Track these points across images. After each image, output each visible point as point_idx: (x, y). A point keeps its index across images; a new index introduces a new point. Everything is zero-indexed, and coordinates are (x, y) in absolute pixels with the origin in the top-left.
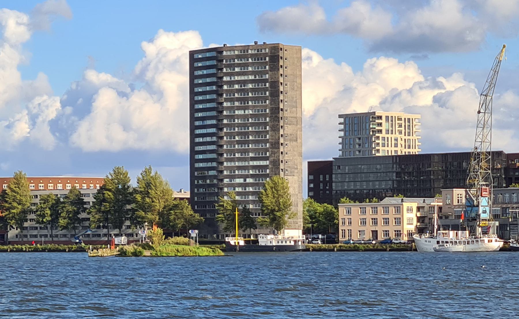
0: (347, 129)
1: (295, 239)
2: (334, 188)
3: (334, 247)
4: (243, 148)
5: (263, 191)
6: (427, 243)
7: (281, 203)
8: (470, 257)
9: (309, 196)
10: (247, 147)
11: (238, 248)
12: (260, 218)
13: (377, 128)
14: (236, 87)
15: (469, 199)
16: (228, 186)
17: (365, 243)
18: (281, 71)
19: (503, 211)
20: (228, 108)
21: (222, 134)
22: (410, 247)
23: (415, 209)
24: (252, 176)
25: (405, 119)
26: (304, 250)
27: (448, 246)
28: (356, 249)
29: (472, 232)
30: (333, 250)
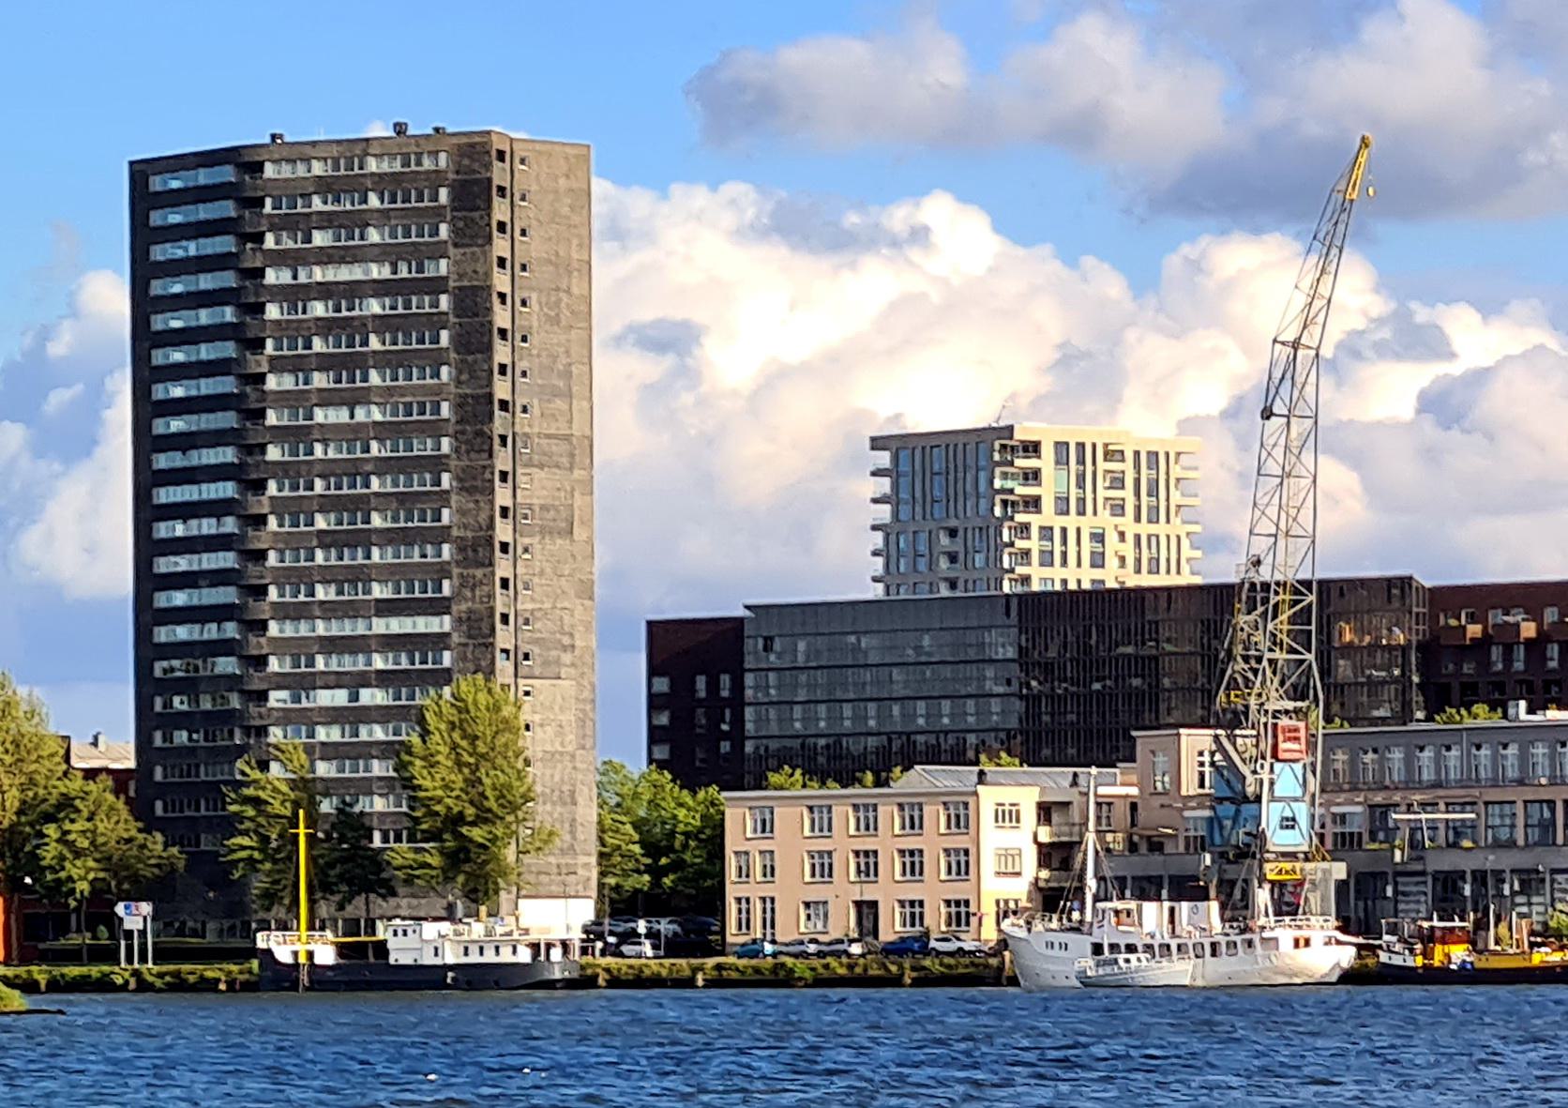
0: (904, 495)
1: (533, 937)
2: (749, 726)
3: (695, 970)
4: (346, 562)
5: (416, 740)
6: (1056, 952)
7: (489, 793)
8: (1209, 1011)
9: (651, 761)
10: (360, 561)
11: (304, 978)
12: (401, 852)
13: (1021, 490)
14: (318, 309)
15: (1227, 774)
16: (286, 718)
17: (820, 955)
18: (500, 246)
19: (1372, 820)
20: (284, 398)
21: (260, 505)
22: (988, 972)
23: (1029, 815)
24: (383, 679)
25: (1137, 454)
26: (569, 984)
27: (1134, 963)
28: (781, 978)
29: (1237, 908)
30: (689, 983)
